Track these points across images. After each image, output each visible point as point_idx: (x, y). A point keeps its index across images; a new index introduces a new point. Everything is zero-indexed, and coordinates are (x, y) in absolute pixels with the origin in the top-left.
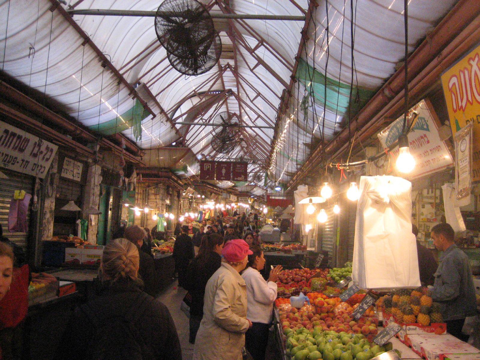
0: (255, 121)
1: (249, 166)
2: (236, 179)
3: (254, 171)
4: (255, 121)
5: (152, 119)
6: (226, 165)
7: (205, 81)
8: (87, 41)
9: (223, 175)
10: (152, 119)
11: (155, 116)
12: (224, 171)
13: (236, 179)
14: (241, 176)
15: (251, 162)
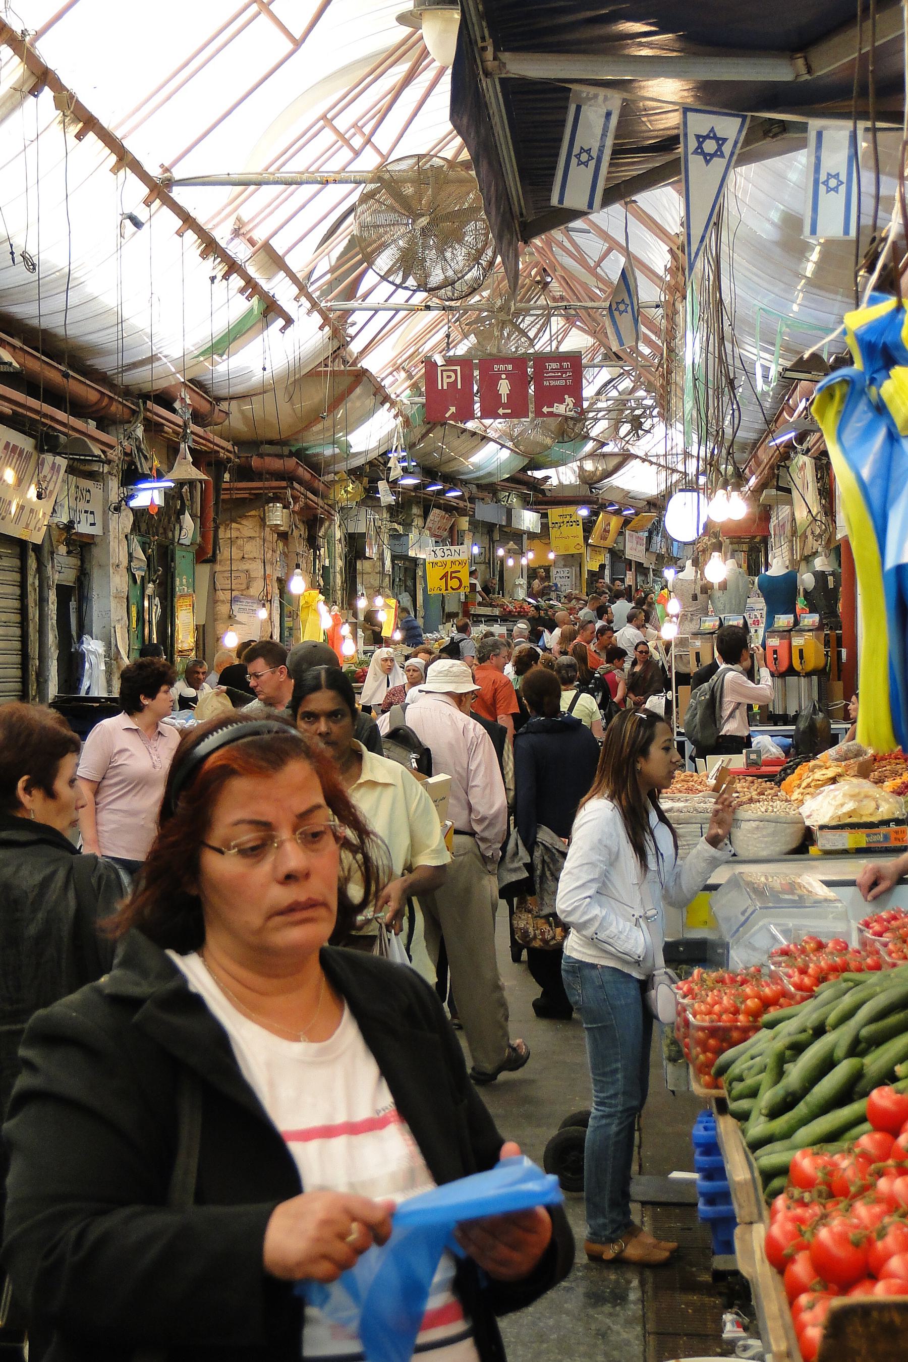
0: (598, 264)
1: (588, 374)
2: (545, 410)
3: (614, 393)
4: (598, 264)
5: (283, 329)
6: (510, 367)
7: (265, 218)
8: (188, 221)
9: (504, 399)
10: (283, 329)
11: (289, 321)
12: (504, 387)
13: (545, 410)
14: (562, 401)
15: (599, 358)
